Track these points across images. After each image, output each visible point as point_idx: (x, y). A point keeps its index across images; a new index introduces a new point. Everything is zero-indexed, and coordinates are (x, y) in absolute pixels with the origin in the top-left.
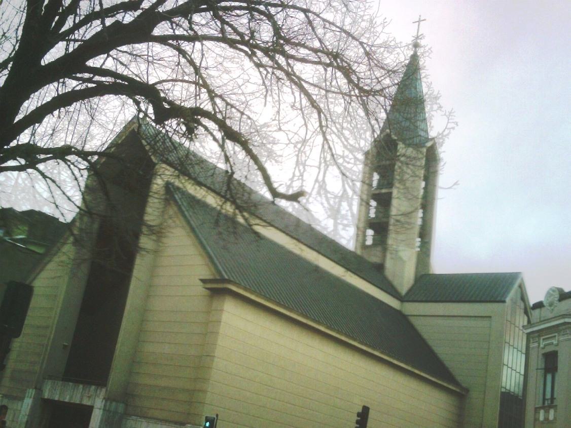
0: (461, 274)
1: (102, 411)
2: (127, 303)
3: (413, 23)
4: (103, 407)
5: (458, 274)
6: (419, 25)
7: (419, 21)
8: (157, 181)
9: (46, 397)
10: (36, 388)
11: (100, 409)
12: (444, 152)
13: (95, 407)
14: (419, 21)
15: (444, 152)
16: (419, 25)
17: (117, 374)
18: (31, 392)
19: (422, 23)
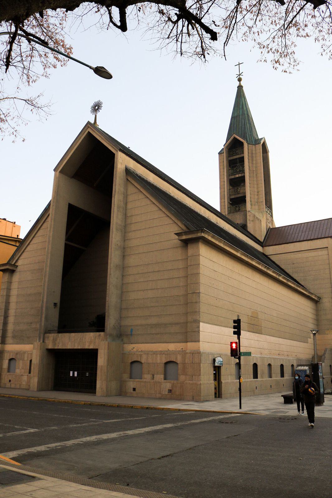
7: (239, 64)
14: (239, 64)
17: (111, 322)
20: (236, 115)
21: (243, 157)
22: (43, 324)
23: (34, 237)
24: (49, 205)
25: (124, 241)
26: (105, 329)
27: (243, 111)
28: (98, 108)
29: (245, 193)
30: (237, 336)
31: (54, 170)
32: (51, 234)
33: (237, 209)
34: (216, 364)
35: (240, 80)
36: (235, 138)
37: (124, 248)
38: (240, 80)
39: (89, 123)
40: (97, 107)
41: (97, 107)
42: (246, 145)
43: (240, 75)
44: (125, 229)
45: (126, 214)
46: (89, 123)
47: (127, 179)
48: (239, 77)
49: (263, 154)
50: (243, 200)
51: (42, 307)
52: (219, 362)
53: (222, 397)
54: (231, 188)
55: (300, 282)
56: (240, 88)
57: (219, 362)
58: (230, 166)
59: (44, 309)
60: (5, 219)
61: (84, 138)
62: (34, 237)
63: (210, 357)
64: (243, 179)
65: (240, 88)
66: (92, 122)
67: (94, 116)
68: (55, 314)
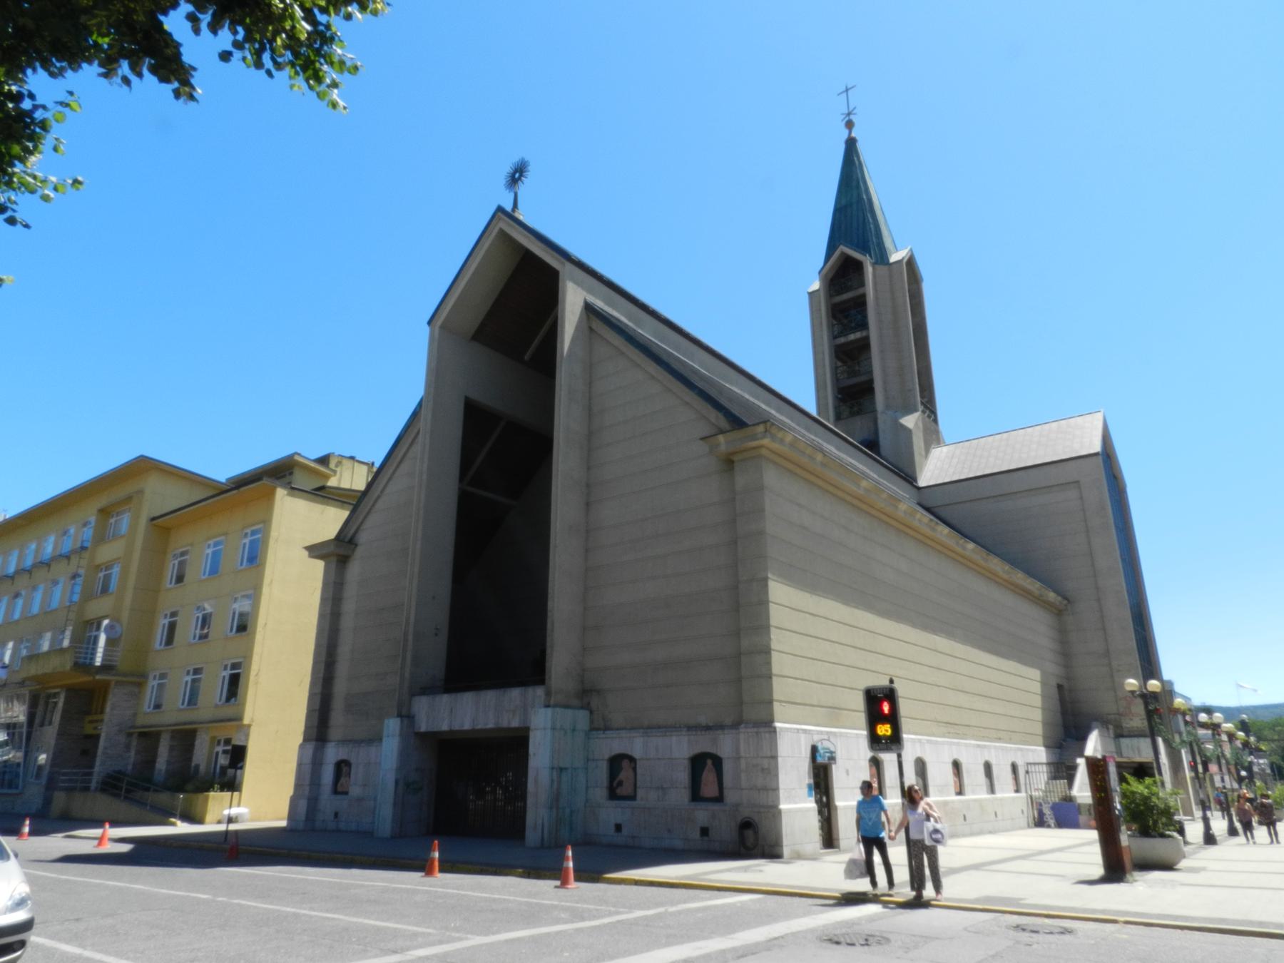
0: (285, 457)
1: (549, 732)
2: (266, 576)
3: (839, 95)
4: (549, 725)
5: (265, 465)
6: (847, 95)
7: (847, 90)
8: (12, 144)
9: (423, 729)
10: (400, 715)
11: (545, 729)
12: (855, 108)
13: (532, 727)
14: (847, 90)
15: (855, 108)
16: (847, 95)
17: (560, 660)
18: (392, 726)
19: (850, 92)
20: (844, 202)
21: (863, 296)
22: (407, 675)
23: (390, 479)
24: (420, 404)
25: (589, 468)
26: (547, 677)
27: (859, 196)
28: (521, 175)
29: (871, 372)
30: (354, 487)
31: (430, 323)
32: (425, 466)
33: (856, 409)
34: (819, 760)
35: (850, 125)
36: (843, 254)
37: (588, 486)
38: (850, 125)
39: (500, 209)
40: (517, 175)
41: (517, 175)
42: (869, 270)
43: (849, 114)
44: (590, 442)
45: (590, 409)
46: (500, 209)
47: (591, 329)
48: (847, 119)
49: (909, 285)
50: (867, 389)
51: (406, 634)
52: (827, 752)
53: (838, 847)
54: (839, 364)
55: (876, 631)
56: (851, 145)
57: (827, 752)
58: (834, 316)
59: (410, 638)
60: (352, 458)
61: (491, 245)
62: (390, 479)
63: (803, 742)
64: (864, 345)
65: (851, 145)
66: (509, 208)
67: (512, 196)
68: (437, 649)
